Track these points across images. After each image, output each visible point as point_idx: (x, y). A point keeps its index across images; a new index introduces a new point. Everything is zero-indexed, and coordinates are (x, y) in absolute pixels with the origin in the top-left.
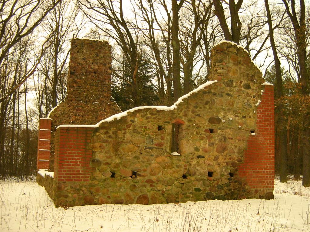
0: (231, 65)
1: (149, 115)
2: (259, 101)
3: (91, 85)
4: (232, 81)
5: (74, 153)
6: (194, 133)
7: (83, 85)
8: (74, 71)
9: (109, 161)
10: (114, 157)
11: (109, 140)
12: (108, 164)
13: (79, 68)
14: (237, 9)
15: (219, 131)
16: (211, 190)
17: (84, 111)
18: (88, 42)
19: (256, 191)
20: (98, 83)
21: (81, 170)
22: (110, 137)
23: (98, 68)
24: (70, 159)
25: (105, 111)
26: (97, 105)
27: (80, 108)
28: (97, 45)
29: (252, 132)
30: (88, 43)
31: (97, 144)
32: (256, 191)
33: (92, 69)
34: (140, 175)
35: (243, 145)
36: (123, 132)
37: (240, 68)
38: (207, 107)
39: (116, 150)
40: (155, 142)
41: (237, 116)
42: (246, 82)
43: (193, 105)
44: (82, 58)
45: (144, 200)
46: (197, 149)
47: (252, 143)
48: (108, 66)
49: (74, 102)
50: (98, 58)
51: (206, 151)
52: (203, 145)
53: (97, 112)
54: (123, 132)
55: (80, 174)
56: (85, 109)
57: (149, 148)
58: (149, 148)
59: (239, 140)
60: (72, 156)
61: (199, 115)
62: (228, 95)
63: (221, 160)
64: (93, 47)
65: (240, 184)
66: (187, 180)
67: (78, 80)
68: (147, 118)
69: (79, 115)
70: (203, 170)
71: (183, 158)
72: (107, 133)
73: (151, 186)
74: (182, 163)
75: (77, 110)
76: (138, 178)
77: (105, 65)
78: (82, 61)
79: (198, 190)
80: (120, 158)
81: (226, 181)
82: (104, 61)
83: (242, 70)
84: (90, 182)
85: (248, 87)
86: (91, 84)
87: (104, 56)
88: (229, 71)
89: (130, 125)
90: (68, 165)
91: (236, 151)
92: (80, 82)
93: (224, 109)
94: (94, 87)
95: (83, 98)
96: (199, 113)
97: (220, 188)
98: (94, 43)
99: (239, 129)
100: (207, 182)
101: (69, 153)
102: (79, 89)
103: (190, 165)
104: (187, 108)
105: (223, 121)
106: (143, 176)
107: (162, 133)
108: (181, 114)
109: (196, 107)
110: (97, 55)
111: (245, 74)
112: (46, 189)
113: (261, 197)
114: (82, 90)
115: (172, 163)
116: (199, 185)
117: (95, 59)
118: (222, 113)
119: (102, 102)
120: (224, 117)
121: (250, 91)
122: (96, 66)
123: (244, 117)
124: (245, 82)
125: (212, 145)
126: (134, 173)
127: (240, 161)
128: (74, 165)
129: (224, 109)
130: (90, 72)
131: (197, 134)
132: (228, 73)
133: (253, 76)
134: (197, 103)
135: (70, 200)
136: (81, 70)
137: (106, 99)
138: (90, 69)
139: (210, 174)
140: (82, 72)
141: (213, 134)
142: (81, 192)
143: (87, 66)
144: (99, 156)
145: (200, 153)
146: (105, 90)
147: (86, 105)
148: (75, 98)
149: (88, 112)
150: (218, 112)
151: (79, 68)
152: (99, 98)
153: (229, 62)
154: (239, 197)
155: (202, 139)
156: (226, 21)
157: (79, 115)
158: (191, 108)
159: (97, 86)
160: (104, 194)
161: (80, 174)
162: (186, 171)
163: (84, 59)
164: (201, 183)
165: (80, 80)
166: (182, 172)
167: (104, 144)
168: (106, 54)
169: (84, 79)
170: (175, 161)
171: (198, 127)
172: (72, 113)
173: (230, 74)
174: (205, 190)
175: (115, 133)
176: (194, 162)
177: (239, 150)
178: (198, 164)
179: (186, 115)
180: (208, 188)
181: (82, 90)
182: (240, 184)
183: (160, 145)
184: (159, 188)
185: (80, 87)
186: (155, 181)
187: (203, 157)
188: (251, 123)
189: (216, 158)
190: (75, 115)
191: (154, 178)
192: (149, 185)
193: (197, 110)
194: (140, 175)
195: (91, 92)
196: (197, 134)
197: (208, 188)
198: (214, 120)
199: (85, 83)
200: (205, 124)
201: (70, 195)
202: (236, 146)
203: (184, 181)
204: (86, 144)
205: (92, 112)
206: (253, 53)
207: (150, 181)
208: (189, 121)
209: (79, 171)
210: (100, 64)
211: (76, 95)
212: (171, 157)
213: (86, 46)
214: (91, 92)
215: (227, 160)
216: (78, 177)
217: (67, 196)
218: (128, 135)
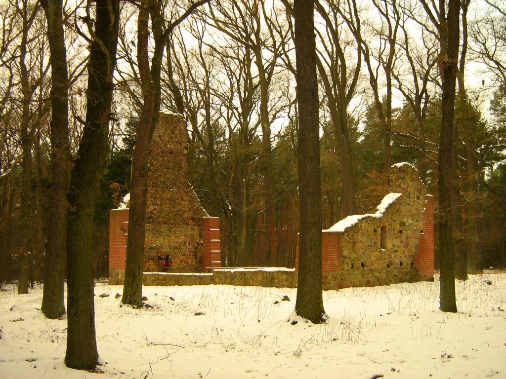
0: (409, 181)
1: (369, 221)
2: (425, 209)
3: (168, 169)
4: (410, 194)
5: (333, 251)
6: (392, 234)
7: (160, 167)
8: (150, 151)
9: (350, 256)
10: (352, 253)
11: (350, 240)
12: (350, 258)
13: (155, 148)
14: (347, 101)
15: (405, 232)
16: (402, 275)
17: (162, 199)
18: (163, 116)
19: (425, 276)
20: (175, 165)
21: (336, 262)
22: (350, 238)
23: (174, 148)
24: (331, 255)
25: (182, 199)
26: (174, 192)
27: (158, 196)
28: (172, 120)
29: (422, 232)
30: (163, 118)
31: (344, 244)
32: (425, 276)
33: (168, 148)
34: (366, 266)
35: (417, 242)
36: (357, 234)
37: (414, 184)
38: (398, 214)
39: (353, 248)
40: (373, 241)
41: (413, 220)
42: (417, 194)
43: (391, 213)
44: (158, 135)
45: (369, 284)
46: (394, 246)
47: (422, 240)
48: (184, 145)
49: (151, 188)
50: (173, 136)
51: (398, 247)
52: (397, 242)
53: (174, 201)
54: (357, 234)
55: (336, 266)
56: (163, 196)
57: (370, 246)
58: (370, 246)
59: (415, 238)
60: (332, 253)
61: (394, 220)
62: (408, 204)
63: (406, 254)
64: (168, 122)
65: (417, 271)
66: (390, 269)
67: (155, 162)
68: (369, 224)
69: (157, 204)
70: (397, 261)
71: (387, 253)
72: (348, 235)
73: (372, 273)
74: (386, 256)
75: (155, 198)
76: (365, 268)
77: (181, 144)
78: (158, 139)
79: (395, 275)
80: (356, 254)
81: (409, 269)
82: (179, 139)
83: (415, 185)
84: (342, 271)
85: (418, 198)
86: (168, 167)
87: (179, 133)
88: (408, 186)
89: (360, 229)
90: (331, 260)
91: (414, 246)
92: (157, 164)
93: (406, 216)
94: (171, 171)
95: (160, 183)
96: (394, 219)
97: (406, 274)
98: (169, 118)
99: (415, 230)
100: (400, 270)
101: (331, 251)
102: (156, 173)
103: (391, 257)
104: (388, 215)
105: (407, 224)
106: (368, 267)
107: (376, 235)
108: (386, 219)
109: (392, 214)
110: (173, 133)
111: (417, 188)
112: (222, 284)
113: (427, 280)
114: (159, 174)
115: (382, 256)
116: (396, 272)
117: (171, 138)
118: (406, 219)
119: (179, 188)
120: (407, 221)
121: (420, 201)
122: (172, 145)
123: (417, 221)
124: (416, 194)
125: (401, 242)
126: (363, 265)
127: (416, 254)
128: (333, 260)
129: (406, 216)
130: (166, 152)
131: (394, 234)
132: (407, 188)
133: (421, 189)
134: (392, 211)
135: (332, 285)
136: (157, 150)
137: (183, 185)
138: (166, 149)
139: (401, 264)
140: (158, 153)
141: (402, 234)
142: (337, 280)
143: (163, 145)
144: (345, 253)
145: (395, 249)
146: (182, 174)
147: (164, 191)
148: (153, 183)
149: (166, 201)
150: (404, 218)
151: (155, 148)
152: (176, 184)
153: (408, 180)
154: (416, 281)
155: (396, 238)
156: (258, 74)
157: (157, 204)
158: (390, 215)
159: (174, 169)
160: (348, 280)
161: (336, 266)
162: (389, 262)
163: (160, 137)
164: (397, 270)
165: (156, 162)
166: (387, 262)
167: (347, 244)
168: (182, 131)
169: (160, 161)
170: (383, 255)
171: (394, 229)
172: (149, 202)
173: (409, 189)
174: (399, 275)
175: (353, 235)
176: (393, 256)
177: (416, 245)
178: (395, 257)
179: (387, 221)
180: (400, 274)
181: (159, 174)
182: (417, 271)
183: (375, 243)
184: (376, 275)
185: (156, 170)
186: (374, 269)
187: (397, 251)
188: (421, 225)
189: (404, 252)
190: (153, 204)
191: (373, 267)
192: (370, 273)
193: (393, 216)
194: (366, 266)
195: (168, 176)
196: (394, 234)
197: (400, 274)
198: (402, 224)
199: (162, 165)
200: (398, 227)
201: (332, 282)
202: (414, 242)
203: (388, 269)
204: (339, 243)
205: (170, 200)
206: (270, 114)
207: (371, 270)
208: (389, 225)
209: (335, 264)
210: (175, 143)
211: (153, 180)
212: (381, 252)
213: (161, 121)
214: (168, 176)
215: (409, 254)
216: (335, 269)
217: (330, 283)
218: (359, 237)
